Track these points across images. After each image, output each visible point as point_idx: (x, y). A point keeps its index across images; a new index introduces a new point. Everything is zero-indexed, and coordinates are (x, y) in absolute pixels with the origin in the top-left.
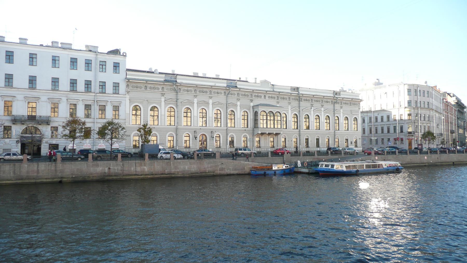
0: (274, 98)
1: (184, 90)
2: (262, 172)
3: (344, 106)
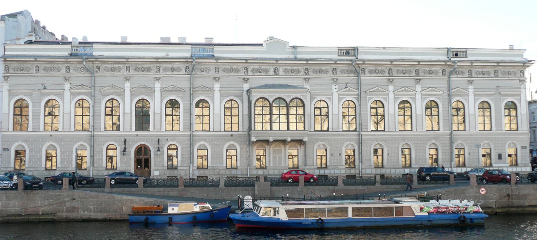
0: (298, 71)
1: (106, 69)
2: (142, 218)
3: (477, 79)
